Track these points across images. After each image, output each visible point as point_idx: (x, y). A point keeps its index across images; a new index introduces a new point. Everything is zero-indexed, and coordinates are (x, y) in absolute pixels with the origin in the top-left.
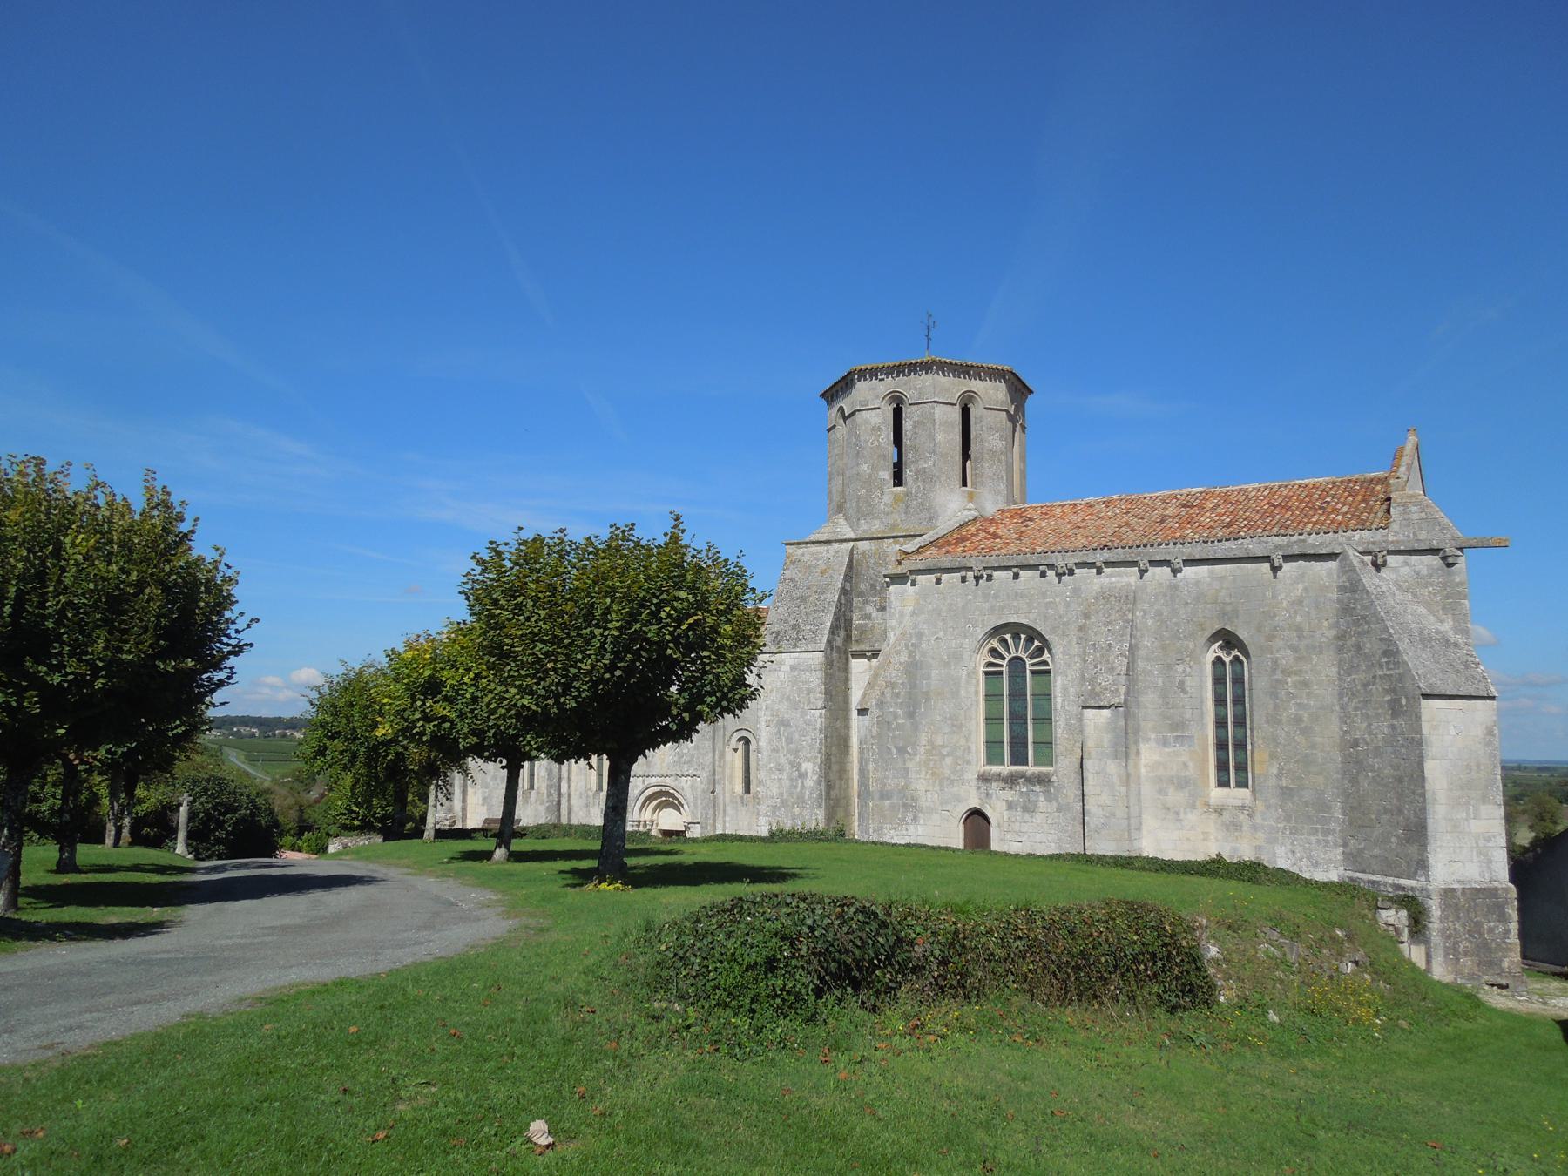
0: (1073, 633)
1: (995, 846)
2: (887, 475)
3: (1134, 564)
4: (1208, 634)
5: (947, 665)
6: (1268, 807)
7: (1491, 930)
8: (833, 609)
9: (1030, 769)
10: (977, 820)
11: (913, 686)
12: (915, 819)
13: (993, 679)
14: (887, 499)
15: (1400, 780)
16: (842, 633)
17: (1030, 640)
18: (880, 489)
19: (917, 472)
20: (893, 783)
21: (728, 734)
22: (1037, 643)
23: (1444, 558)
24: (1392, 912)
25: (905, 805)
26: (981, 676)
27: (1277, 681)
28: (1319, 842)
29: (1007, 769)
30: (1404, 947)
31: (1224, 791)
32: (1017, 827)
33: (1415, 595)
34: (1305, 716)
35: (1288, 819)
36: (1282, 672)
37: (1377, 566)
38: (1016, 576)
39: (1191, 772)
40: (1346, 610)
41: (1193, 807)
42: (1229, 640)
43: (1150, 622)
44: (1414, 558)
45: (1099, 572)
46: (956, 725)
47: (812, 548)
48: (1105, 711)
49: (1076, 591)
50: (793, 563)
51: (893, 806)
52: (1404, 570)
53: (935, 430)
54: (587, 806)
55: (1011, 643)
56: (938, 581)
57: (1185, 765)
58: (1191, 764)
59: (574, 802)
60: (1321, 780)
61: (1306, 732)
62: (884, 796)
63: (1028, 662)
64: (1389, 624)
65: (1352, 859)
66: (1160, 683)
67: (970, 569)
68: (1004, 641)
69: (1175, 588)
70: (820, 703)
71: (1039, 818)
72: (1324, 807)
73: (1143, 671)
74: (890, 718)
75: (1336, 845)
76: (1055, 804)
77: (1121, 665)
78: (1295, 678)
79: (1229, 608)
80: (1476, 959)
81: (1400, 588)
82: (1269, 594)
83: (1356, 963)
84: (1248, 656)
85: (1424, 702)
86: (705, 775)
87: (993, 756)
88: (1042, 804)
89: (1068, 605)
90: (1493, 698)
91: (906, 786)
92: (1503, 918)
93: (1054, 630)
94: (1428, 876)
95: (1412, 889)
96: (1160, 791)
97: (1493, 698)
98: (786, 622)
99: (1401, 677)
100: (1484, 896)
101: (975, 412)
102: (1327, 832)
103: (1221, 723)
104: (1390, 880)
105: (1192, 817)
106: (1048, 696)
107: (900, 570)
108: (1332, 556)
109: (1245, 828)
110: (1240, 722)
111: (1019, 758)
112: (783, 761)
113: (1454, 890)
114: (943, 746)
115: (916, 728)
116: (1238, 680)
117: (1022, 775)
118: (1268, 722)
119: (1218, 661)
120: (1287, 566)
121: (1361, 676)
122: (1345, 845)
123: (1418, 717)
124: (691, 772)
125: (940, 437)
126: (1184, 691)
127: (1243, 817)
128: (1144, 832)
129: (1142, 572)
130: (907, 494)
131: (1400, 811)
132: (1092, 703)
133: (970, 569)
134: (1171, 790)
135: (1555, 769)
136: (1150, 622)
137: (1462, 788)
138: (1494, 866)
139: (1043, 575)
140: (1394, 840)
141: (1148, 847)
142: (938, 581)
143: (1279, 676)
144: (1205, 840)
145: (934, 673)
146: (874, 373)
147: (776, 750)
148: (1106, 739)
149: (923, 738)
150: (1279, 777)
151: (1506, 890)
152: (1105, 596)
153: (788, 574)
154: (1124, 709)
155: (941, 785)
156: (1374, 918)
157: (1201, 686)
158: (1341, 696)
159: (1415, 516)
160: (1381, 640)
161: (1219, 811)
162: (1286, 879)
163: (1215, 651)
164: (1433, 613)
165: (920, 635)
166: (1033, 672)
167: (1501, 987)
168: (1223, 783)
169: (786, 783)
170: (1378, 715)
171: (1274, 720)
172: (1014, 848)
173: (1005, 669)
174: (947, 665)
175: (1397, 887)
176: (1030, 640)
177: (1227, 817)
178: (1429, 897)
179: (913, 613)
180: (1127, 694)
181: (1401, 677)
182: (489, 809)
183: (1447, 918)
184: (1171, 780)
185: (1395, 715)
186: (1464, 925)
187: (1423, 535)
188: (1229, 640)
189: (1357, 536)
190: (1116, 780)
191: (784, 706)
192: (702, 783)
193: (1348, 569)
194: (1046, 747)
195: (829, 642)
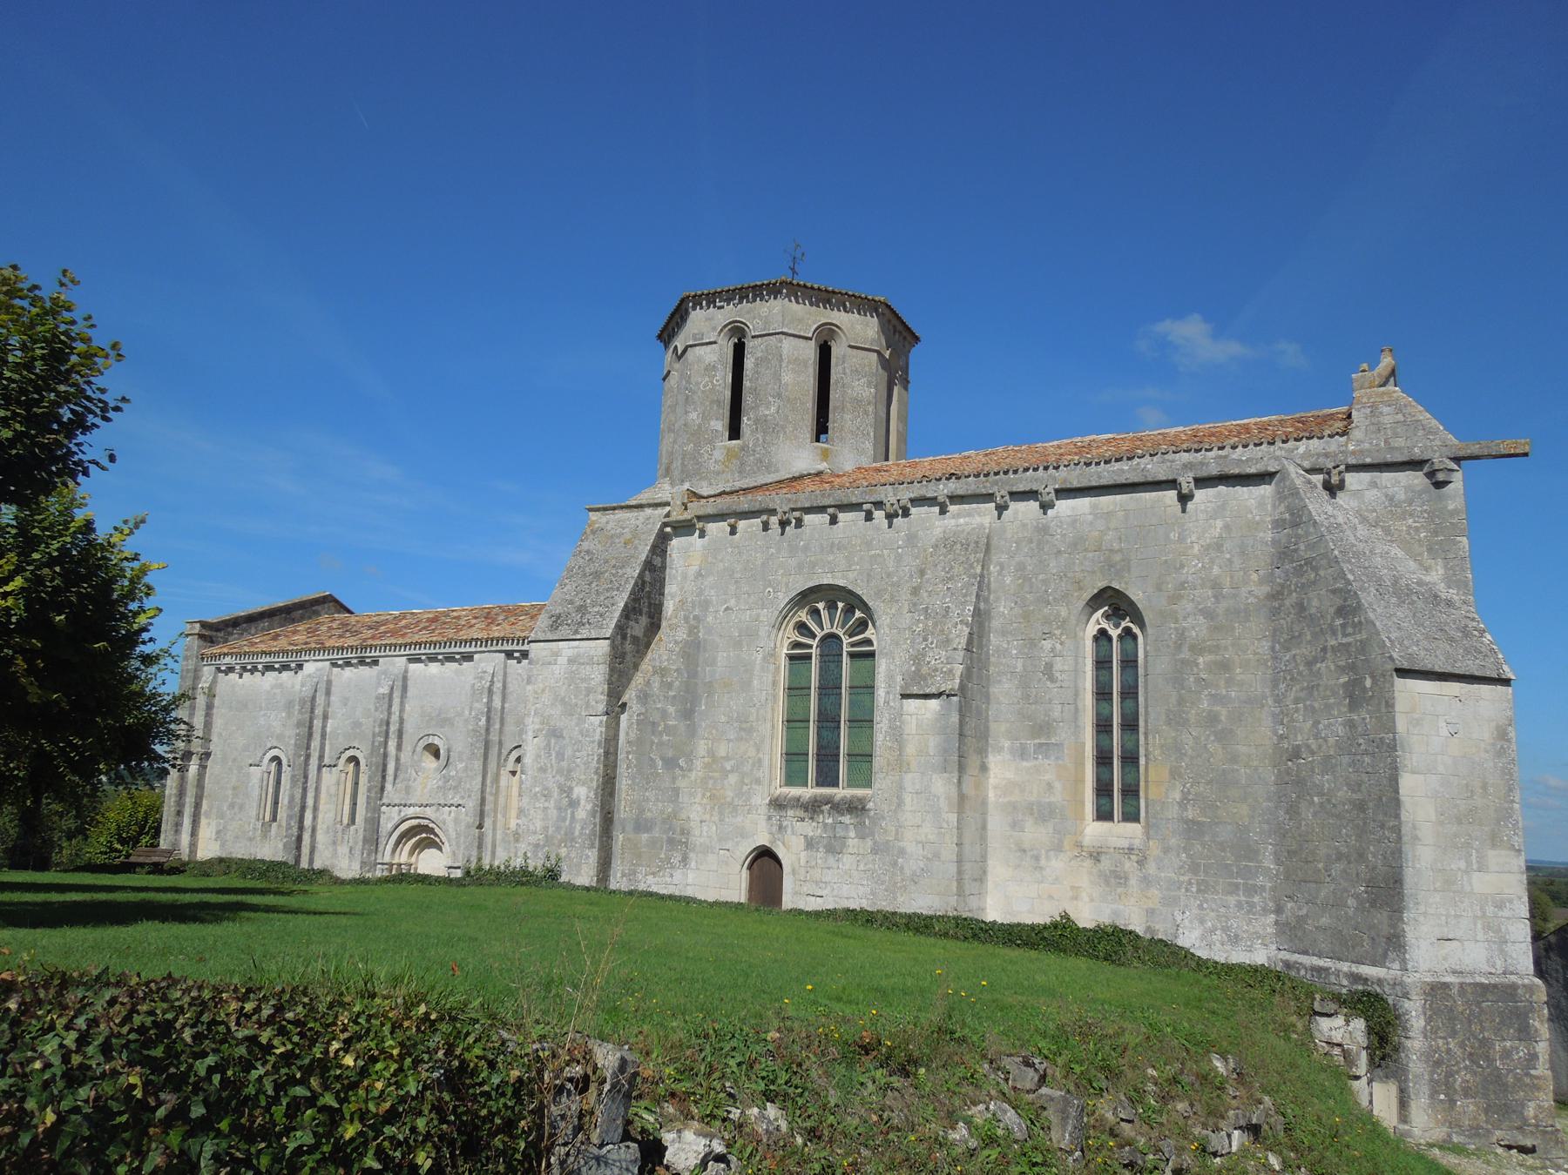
0: (905, 595)
1: (788, 901)
2: (720, 425)
3: (989, 497)
4: (1087, 595)
5: (738, 644)
6: (1166, 850)
7: (1507, 1054)
8: (629, 587)
9: (841, 792)
10: (765, 861)
11: (693, 674)
12: (685, 860)
13: (799, 665)
14: (718, 455)
15: (1361, 806)
16: (644, 620)
17: (849, 610)
18: (711, 442)
19: (757, 421)
20: (655, 808)
21: (505, 752)
22: (858, 614)
23: (1431, 475)
24: (1339, 1021)
25: (671, 841)
26: (783, 662)
27: (1183, 661)
28: (1239, 905)
29: (808, 792)
30: (1360, 1086)
31: (1106, 825)
32: (816, 874)
33: (1387, 531)
34: (1223, 713)
35: (1194, 869)
36: (1192, 648)
37: (1332, 489)
38: (834, 520)
39: (1058, 796)
40: (1284, 554)
41: (1058, 848)
42: (1115, 603)
43: (1008, 580)
44: (1386, 477)
45: (943, 511)
46: (745, 728)
47: (620, 514)
48: (934, 704)
49: (911, 539)
50: (593, 532)
51: (653, 843)
52: (1372, 495)
53: (784, 372)
54: (334, 843)
55: (824, 614)
56: (733, 531)
57: (1050, 786)
58: (1058, 785)
59: (320, 837)
60: (1244, 810)
61: (1224, 736)
62: (641, 825)
63: (846, 640)
64: (1346, 566)
65: (1290, 932)
66: (1019, 668)
67: (773, 512)
68: (815, 613)
69: (1044, 530)
70: (601, 708)
71: (848, 861)
72: (1251, 853)
73: (997, 650)
74: (656, 717)
75: (1265, 911)
76: (869, 843)
77: (960, 636)
78: (1210, 658)
79: (1118, 557)
80: (1483, 1103)
81: (1364, 520)
82: (1173, 536)
83: (1254, 1130)
84: (1142, 626)
85: (1400, 683)
86: (472, 803)
87: (794, 776)
88: (853, 842)
89: (899, 558)
90: (1506, 682)
91: (675, 815)
92: (1525, 1034)
93: (879, 594)
94: (1404, 962)
95: (1380, 982)
96: (1015, 825)
97: (1506, 682)
98: (571, 602)
99: (1363, 646)
100: (1493, 997)
101: (837, 351)
102: (1252, 890)
103: (1103, 727)
104: (1345, 967)
105: (1057, 864)
106: (870, 688)
107: (687, 516)
108: (1263, 477)
109: (1133, 881)
110: (1130, 725)
111: (827, 776)
112: (551, 784)
113: (1446, 986)
114: (727, 758)
115: (692, 732)
116: (1130, 663)
117: (828, 800)
118: (1169, 724)
119: (1102, 635)
120: (1201, 495)
121: (1304, 651)
122: (1279, 910)
123: (1390, 705)
124: (456, 801)
125: (787, 378)
126: (1052, 679)
127: (1129, 865)
128: (990, 885)
129: (1001, 509)
130: (742, 449)
131: (1361, 856)
132: (915, 690)
133: (773, 512)
134: (1029, 824)
135: (1539, 869)
136: (1008, 580)
137: (1460, 822)
138: (1509, 948)
139: (869, 517)
140: (1351, 902)
141: (994, 912)
142: (733, 531)
143: (1185, 654)
144: (1076, 898)
145: (721, 657)
146: (711, 299)
147: (543, 770)
148: (933, 743)
149: (702, 747)
150: (1182, 805)
151: (1530, 989)
152: (947, 543)
153: (585, 545)
154: (967, 699)
155: (721, 813)
156: (1308, 1029)
157: (1077, 671)
158: (1275, 685)
159: (1387, 420)
160: (1334, 592)
161: (1096, 856)
162: (1165, 956)
163: (1097, 621)
164: (1415, 557)
165: (706, 605)
166: (852, 655)
167: (1523, 1150)
168: (1104, 815)
169: (553, 813)
170: (1328, 707)
171: (1177, 720)
172: (812, 905)
173: (814, 651)
174: (738, 644)
175: (1356, 978)
176: (849, 610)
177: (1106, 863)
178: (1406, 996)
179: (699, 575)
180: (967, 676)
181: (1363, 646)
182: (222, 845)
183: (1434, 1031)
184: (1030, 809)
185: (1354, 705)
186: (1462, 1045)
187: (1399, 442)
188: (1115, 603)
189: (1302, 447)
190: (943, 804)
191: (556, 711)
192: (467, 815)
193: (1289, 495)
194: (863, 758)
195: (621, 629)
